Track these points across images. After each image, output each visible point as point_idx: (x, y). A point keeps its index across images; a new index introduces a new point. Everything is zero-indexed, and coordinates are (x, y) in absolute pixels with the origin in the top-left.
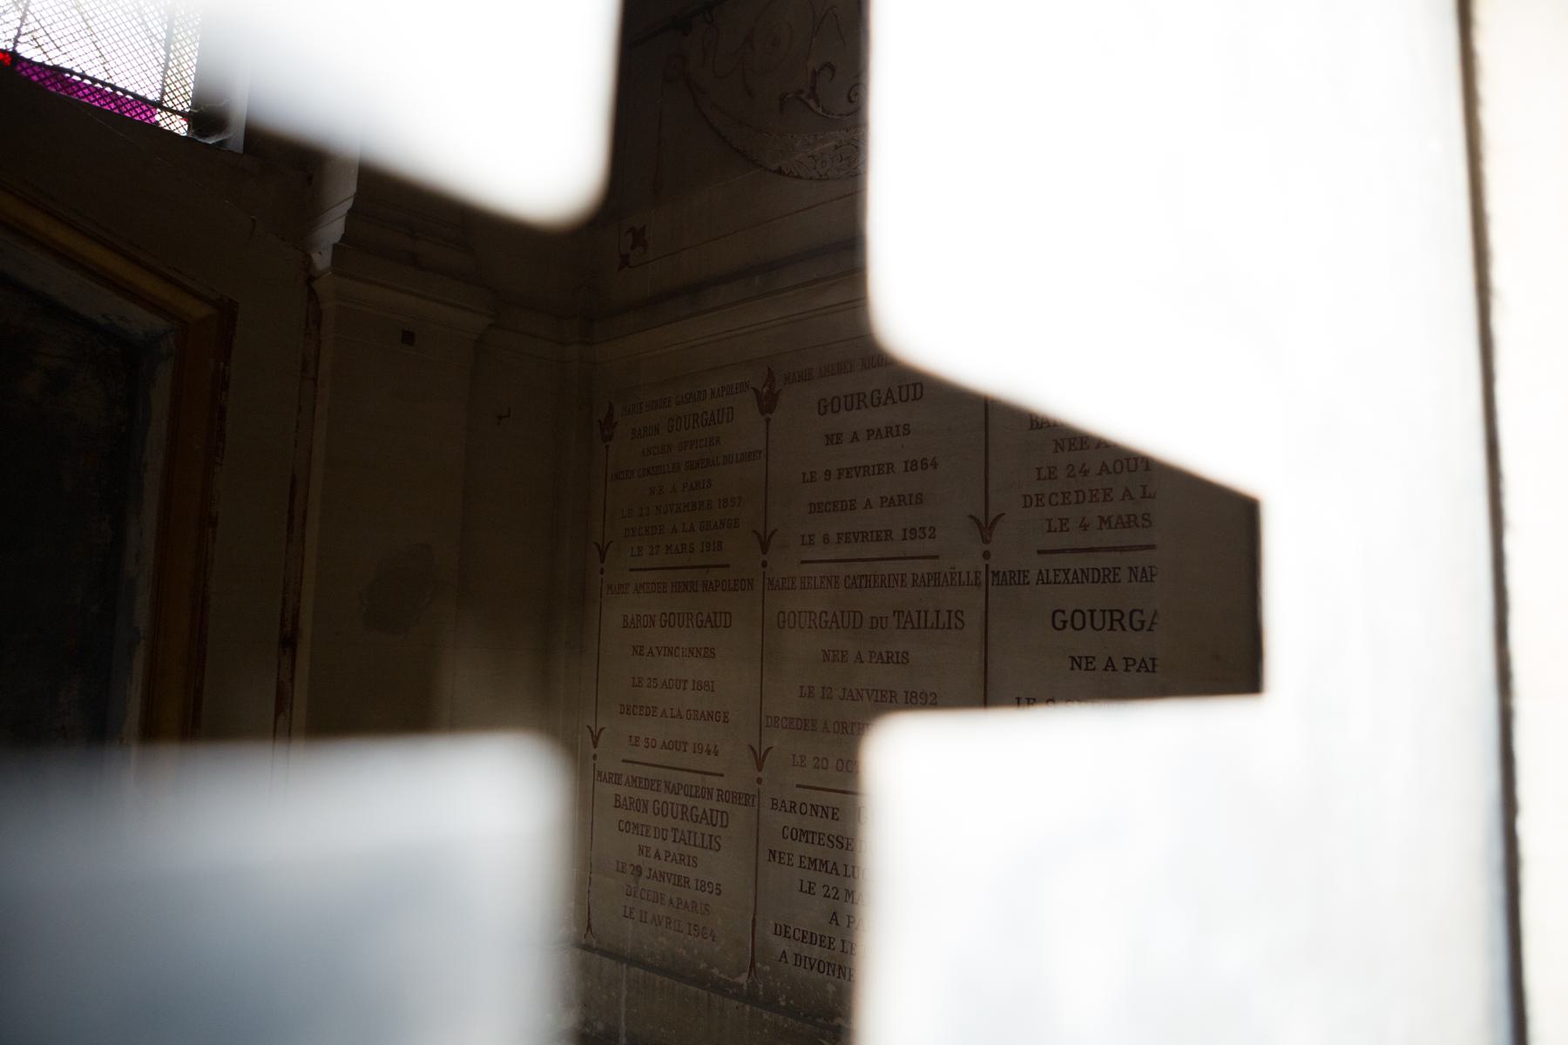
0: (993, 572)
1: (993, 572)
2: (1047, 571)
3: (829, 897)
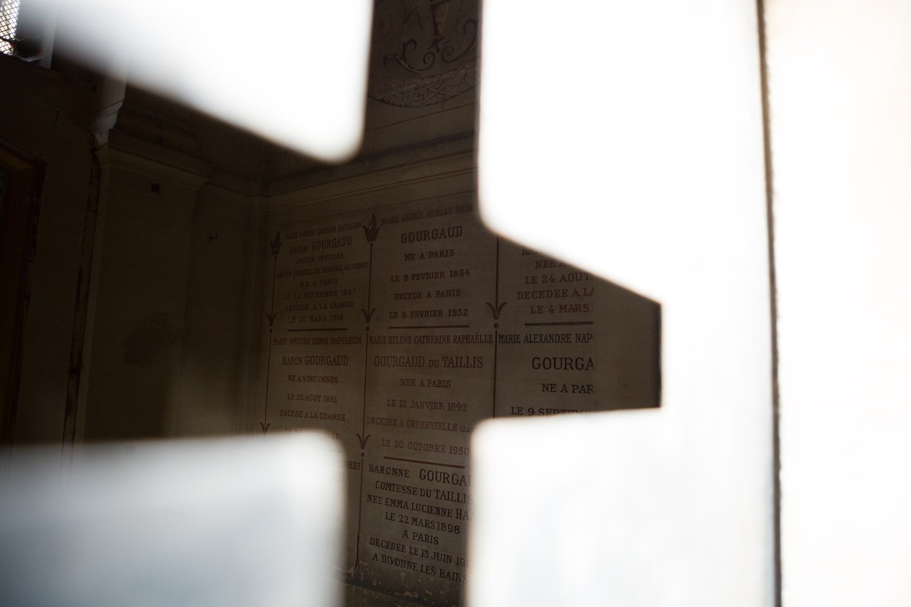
0: (500, 335)
1: (500, 335)
2: (530, 335)
3: (403, 522)
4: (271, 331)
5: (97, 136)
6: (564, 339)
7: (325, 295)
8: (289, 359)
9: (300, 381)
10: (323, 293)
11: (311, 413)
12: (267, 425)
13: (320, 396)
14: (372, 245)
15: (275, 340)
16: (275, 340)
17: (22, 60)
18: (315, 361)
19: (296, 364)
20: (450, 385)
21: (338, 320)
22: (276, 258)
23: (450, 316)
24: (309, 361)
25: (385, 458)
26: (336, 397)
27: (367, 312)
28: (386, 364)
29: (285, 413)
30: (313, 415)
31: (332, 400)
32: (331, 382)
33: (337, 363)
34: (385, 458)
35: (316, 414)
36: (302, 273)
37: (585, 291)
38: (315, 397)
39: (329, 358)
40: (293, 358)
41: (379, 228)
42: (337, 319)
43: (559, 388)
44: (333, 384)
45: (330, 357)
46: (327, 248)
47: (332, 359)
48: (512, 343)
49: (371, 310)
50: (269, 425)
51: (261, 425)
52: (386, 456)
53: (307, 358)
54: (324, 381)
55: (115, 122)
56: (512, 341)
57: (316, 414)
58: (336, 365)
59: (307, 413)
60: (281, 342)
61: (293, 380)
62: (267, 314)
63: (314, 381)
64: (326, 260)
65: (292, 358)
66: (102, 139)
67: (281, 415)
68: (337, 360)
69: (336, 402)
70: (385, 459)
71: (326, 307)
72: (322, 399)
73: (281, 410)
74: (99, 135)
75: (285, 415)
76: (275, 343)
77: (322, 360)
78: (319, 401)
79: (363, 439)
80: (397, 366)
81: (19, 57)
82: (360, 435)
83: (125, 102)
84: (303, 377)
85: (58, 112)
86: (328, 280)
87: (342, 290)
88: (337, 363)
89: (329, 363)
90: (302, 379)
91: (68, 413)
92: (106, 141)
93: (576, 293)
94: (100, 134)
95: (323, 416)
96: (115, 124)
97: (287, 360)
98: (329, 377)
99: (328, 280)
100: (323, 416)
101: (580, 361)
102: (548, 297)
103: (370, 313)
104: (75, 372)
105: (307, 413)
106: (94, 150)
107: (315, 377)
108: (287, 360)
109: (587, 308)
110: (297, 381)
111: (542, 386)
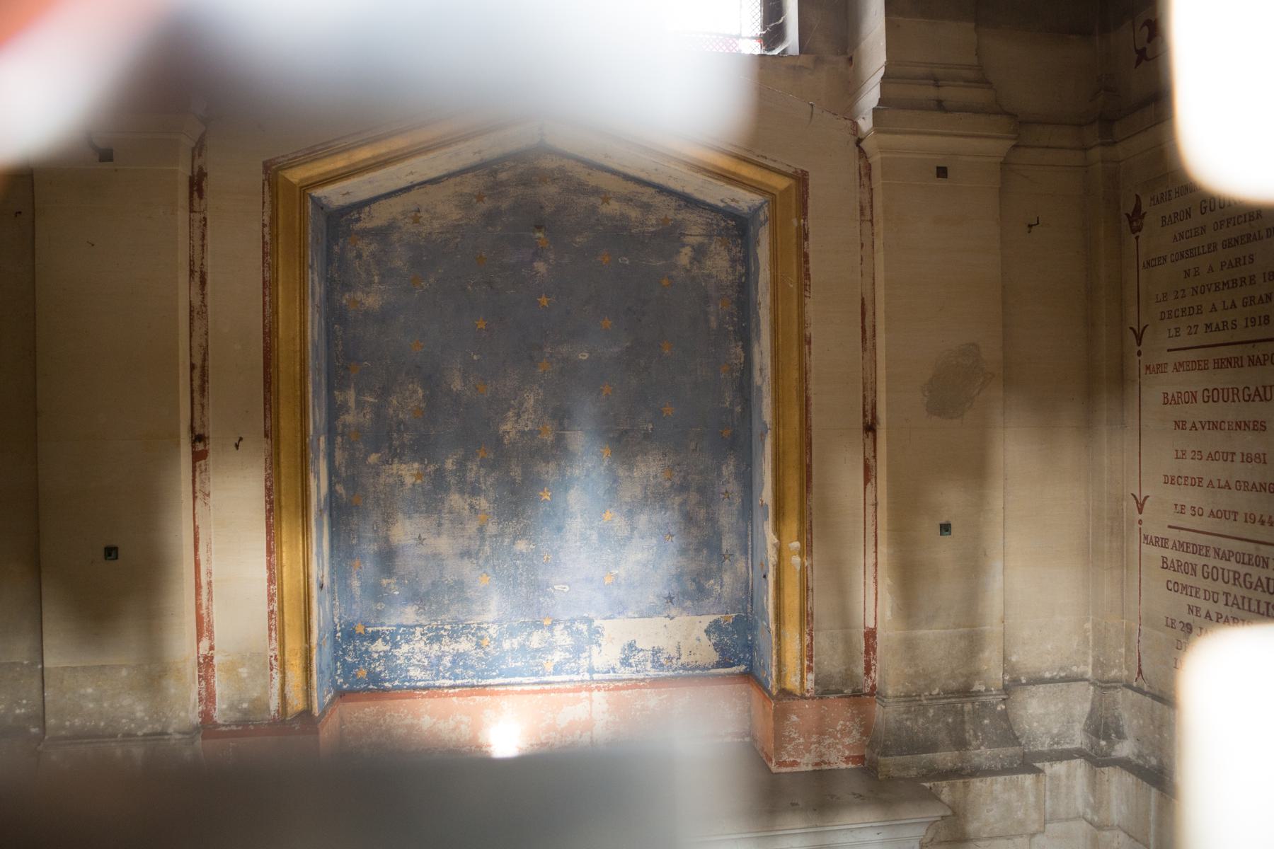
4: (1139, 353)
5: (861, 122)
6: (1237, 362)
7: (1231, 285)
8: (1173, 396)
9: (1196, 430)
10: (1228, 282)
11: (1219, 480)
12: (1142, 499)
13: (1233, 454)
14: (1137, 238)
15: (1148, 368)
16: (1148, 368)
17: (769, 56)
18: (1221, 395)
19: (1187, 403)
20: (1265, 427)
21: (1260, 324)
22: (1137, 238)
23: (1247, 326)
24: (1208, 397)
25: (1170, 527)
26: (1264, 454)
27: (1137, 332)
28: (1221, 398)
29: (1173, 480)
30: (1223, 483)
31: (1258, 460)
32: (1254, 429)
33: (1263, 398)
34: (1170, 527)
35: (1227, 482)
36: (1185, 255)
37: (1224, 304)
38: (1225, 455)
39: (1246, 390)
40: (1180, 393)
41: (1145, 213)
42: (1258, 323)
43: (1189, 426)
44: (1256, 432)
45: (1249, 388)
46: (1187, 218)
47: (1252, 391)
48: (1239, 367)
49: (1141, 328)
50: (1146, 498)
51: (1133, 497)
52: (1171, 524)
53: (1206, 392)
54: (1240, 428)
55: (879, 97)
56: (1238, 365)
57: (1227, 482)
58: (1261, 400)
59: (1211, 481)
60: (1158, 368)
61: (1183, 429)
62: (1131, 328)
63: (1221, 429)
64: (1228, 227)
65: (1178, 393)
66: (866, 124)
67: (1165, 483)
68: (1262, 393)
69: (1265, 463)
70: (1169, 529)
71: (1234, 305)
72: (1238, 458)
73: (1165, 476)
74: (862, 120)
75: (1171, 483)
76: (1148, 372)
77: (1233, 394)
78: (1232, 461)
79: (1140, 499)
80: (1239, 401)
81: (766, 53)
82: (1135, 494)
83: (888, 66)
84: (1201, 422)
85: (812, 105)
86: (1236, 259)
87: (1264, 274)
88: (1263, 398)
89: (1247, 398)
90: (1198, 425)
91: (867, 480)
92: (871, 125)
93: (1214, 309)
94: (863, 118)
95: (1240, 486)
96: (880, 99)
97: (1170, 397)
98: (1179, 421)
99: (1236, 259)
100: (1240, 486)
101: (1247, 392)
102: (1189, 315)
103: (1140, 331)
104: (870, 428)
105: (1211, 481)
106: (859, 141)
107: (1223, 422)
108: (1170, 397)
109: (1235, 324)
110: (1191, 430)
111: (1174, 423)
